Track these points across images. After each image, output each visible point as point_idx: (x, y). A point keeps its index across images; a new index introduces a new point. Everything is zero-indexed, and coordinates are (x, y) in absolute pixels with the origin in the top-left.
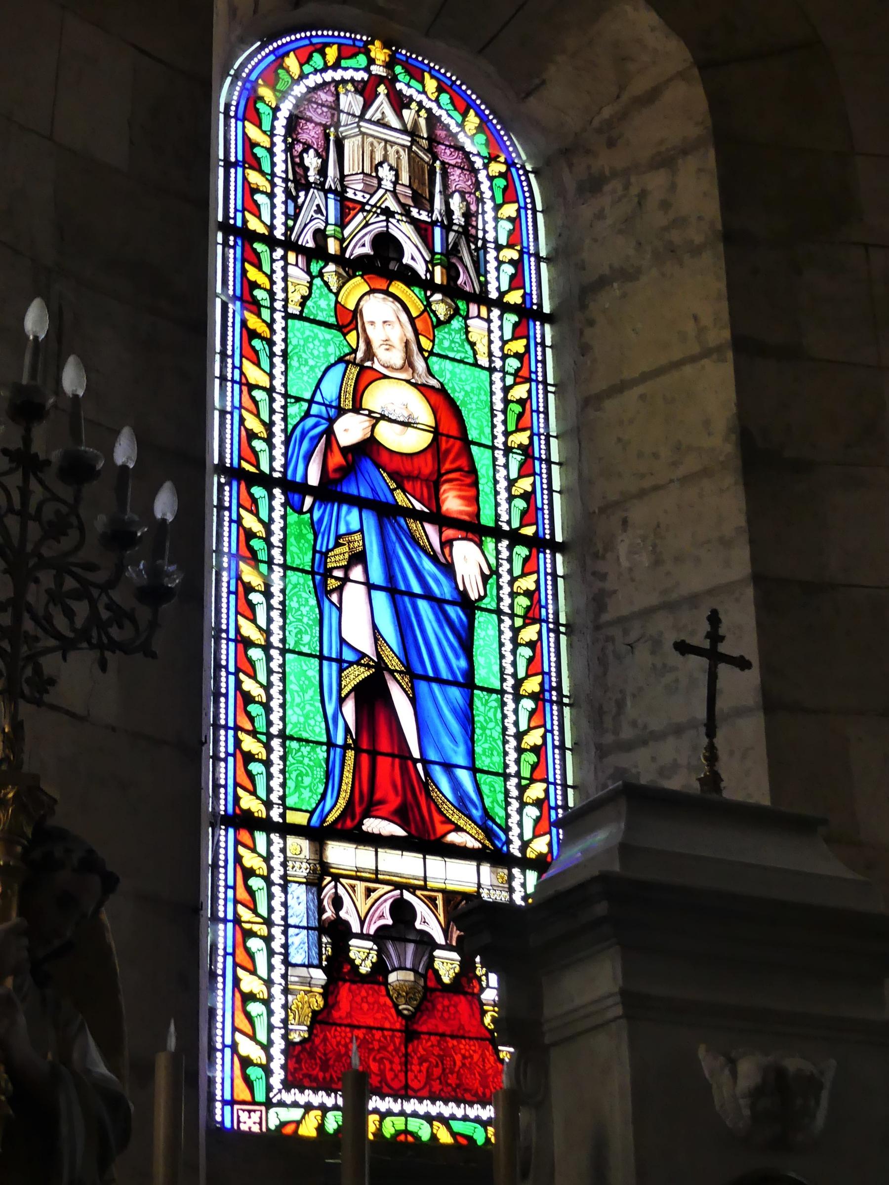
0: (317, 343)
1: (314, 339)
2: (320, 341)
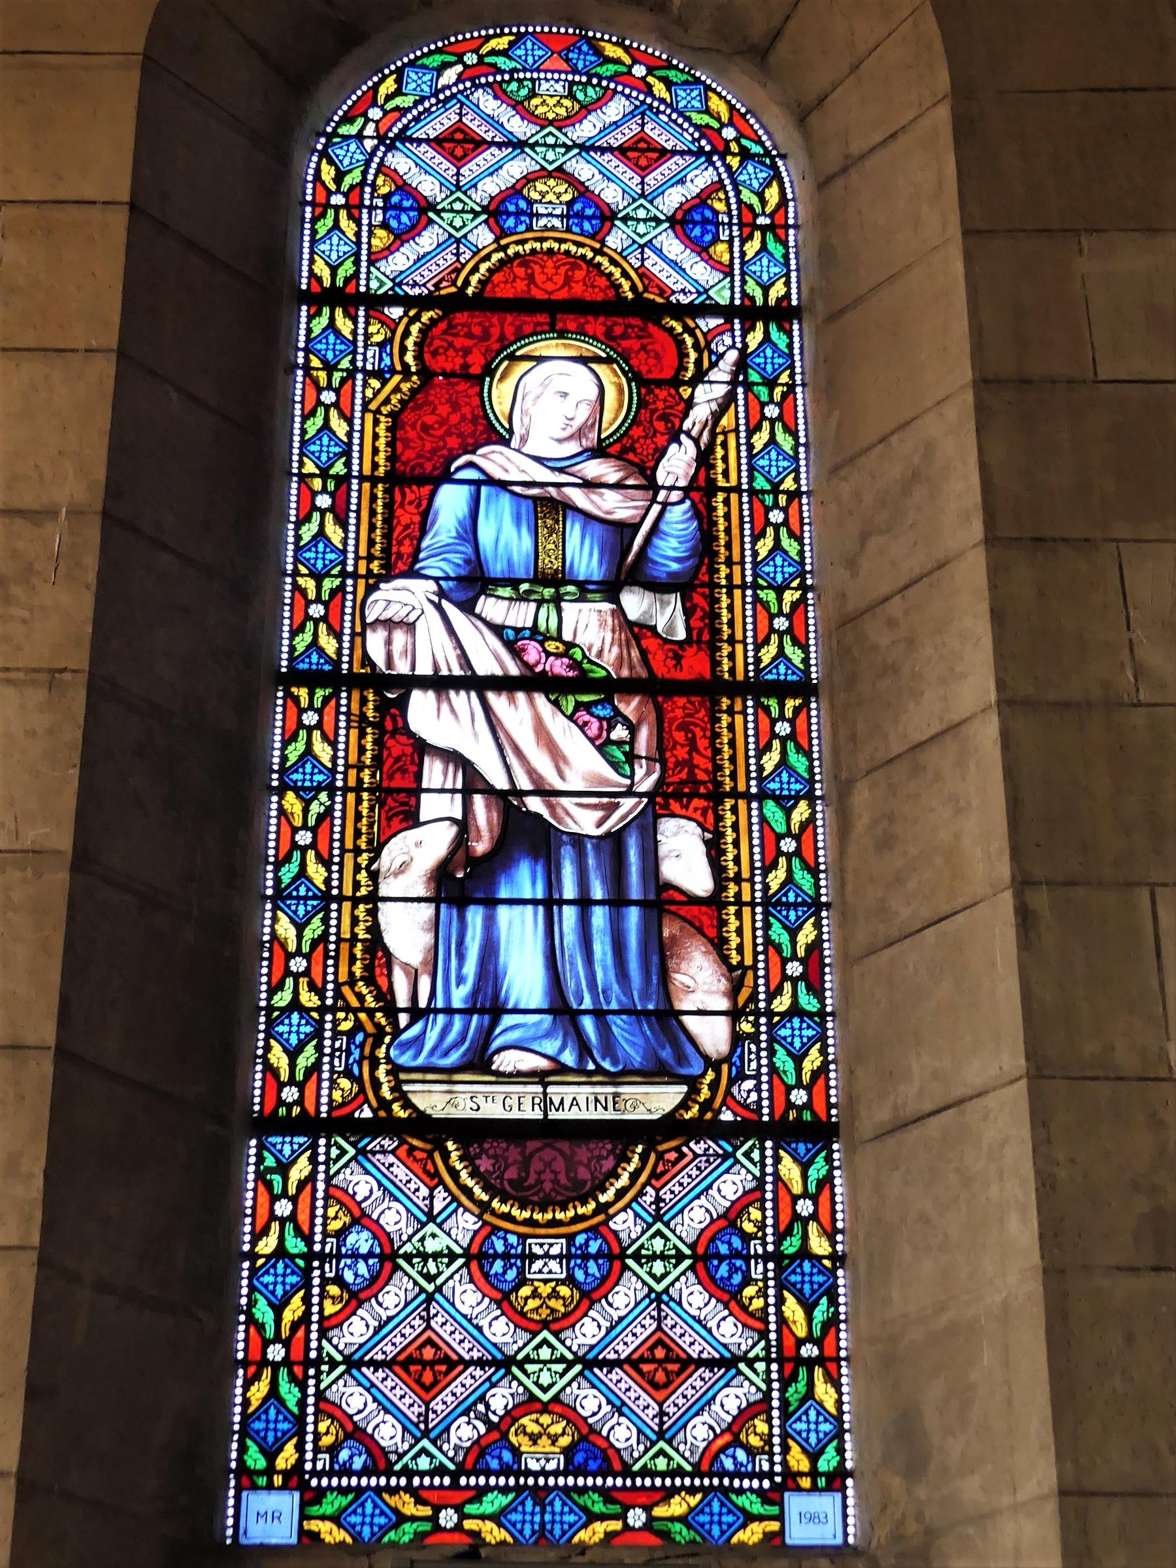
0: (451, 352)
1: (447, 349)
2: (456, 351)
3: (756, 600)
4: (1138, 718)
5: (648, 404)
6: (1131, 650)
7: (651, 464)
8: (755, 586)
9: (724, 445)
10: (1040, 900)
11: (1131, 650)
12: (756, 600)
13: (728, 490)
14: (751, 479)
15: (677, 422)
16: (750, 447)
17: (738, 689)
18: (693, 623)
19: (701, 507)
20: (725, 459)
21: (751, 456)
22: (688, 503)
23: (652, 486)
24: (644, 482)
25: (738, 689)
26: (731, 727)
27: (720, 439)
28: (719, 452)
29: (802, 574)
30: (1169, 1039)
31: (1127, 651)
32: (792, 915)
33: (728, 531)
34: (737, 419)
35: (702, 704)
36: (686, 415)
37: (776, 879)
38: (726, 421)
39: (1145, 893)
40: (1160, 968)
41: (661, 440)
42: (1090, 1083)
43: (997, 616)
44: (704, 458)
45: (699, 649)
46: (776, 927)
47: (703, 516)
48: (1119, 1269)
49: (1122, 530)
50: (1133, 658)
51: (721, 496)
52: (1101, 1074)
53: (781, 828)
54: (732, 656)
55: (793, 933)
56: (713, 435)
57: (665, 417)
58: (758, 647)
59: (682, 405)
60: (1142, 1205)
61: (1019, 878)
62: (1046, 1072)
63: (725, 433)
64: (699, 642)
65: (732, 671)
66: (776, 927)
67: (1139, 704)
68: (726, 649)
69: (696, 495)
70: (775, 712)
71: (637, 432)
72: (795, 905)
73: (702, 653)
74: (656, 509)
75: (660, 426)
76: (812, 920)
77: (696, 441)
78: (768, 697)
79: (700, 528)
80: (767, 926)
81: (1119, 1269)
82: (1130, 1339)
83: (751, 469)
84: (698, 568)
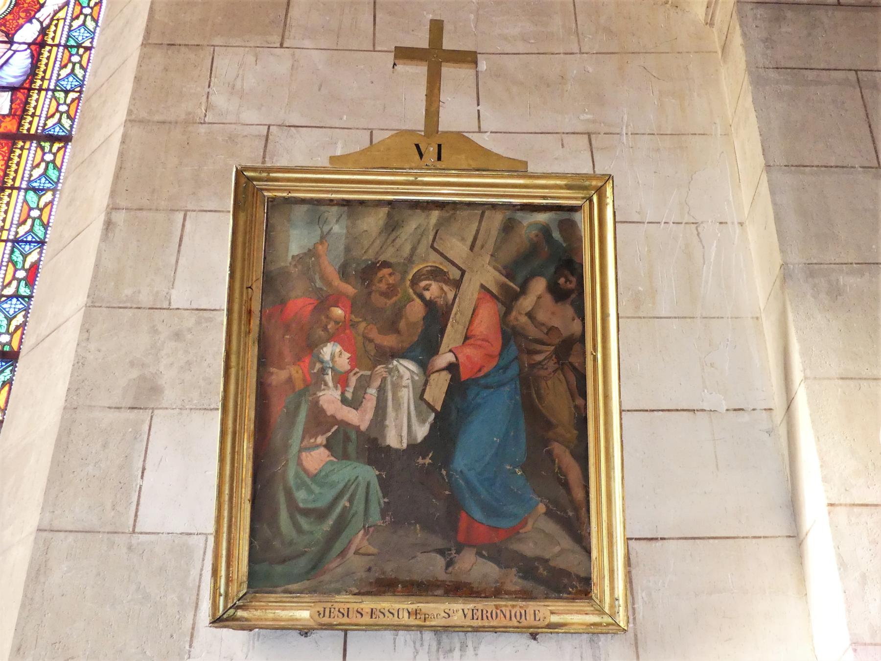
3: (54, 97)
4: (203, 129)
5: (20, 4)
6: (208, 97)
7: (13, 32)
8: (54, 91)
9: (56, 25)
10: (119, 217)
11: (208, 97)
12: (54, 97)
13: (52, 46)
14: (67, 40)
15: (33, 13)
16: (70, 26)
17: (28, 137)
18: (13, 106)
19: (35, 53)
20: (55, 32)
21: (70, 31)
22: (29, 51)
23: (11, 42)
24: (6, 39)
25: (28, 137)
26: (20, 156)
27: (55, 22)
28: (53, 28)
29: (81, 86)
30: (173, 288)
31: (205, 97)
32: (27, 247)
33: (47, 65)
34: (67, 13)
35: (6, 144)
36: (39, 10)
37: (22, 230)
38: (61, 15)
39: (180, 216)
40: (179, 251)
41: (21, 21)
42: (121, 310)
43: (137, 79)
44: (44, 31)
45: (13, 118)
46: (17, 253)
47: (35, 60)
48: (109, 408)
49: (217, 41)
50: (207, 101)
51: (48, 48)
52: (129, 305)
53: (33, 205)
54: (31, 123)
55: (25, 256)
56: (52, 20)
57: (27, 11)
58: (47, 118)
59: (38, 6)
60: (135, 373)
61: (111, 206)
62: (96, 304)
63: (58, 20)
64: (14, 115)
65: (29, 130)
66: (17, 253)
67: (205, 123)
68: (29, 119)
69: (33, 47)
70: (47, 150)
71: (9, 17)
72: (30, 242)
73: (14, 120)
74: (10, 53)
75: (23, 15)
76: (39, 250)
77: (41, 23)
78: (45, 142)
79: (32, 63)
80: (12, 252)
81: (109, 408)
82: (105, 446)
83: (69, 36)
84: (25, 81)
